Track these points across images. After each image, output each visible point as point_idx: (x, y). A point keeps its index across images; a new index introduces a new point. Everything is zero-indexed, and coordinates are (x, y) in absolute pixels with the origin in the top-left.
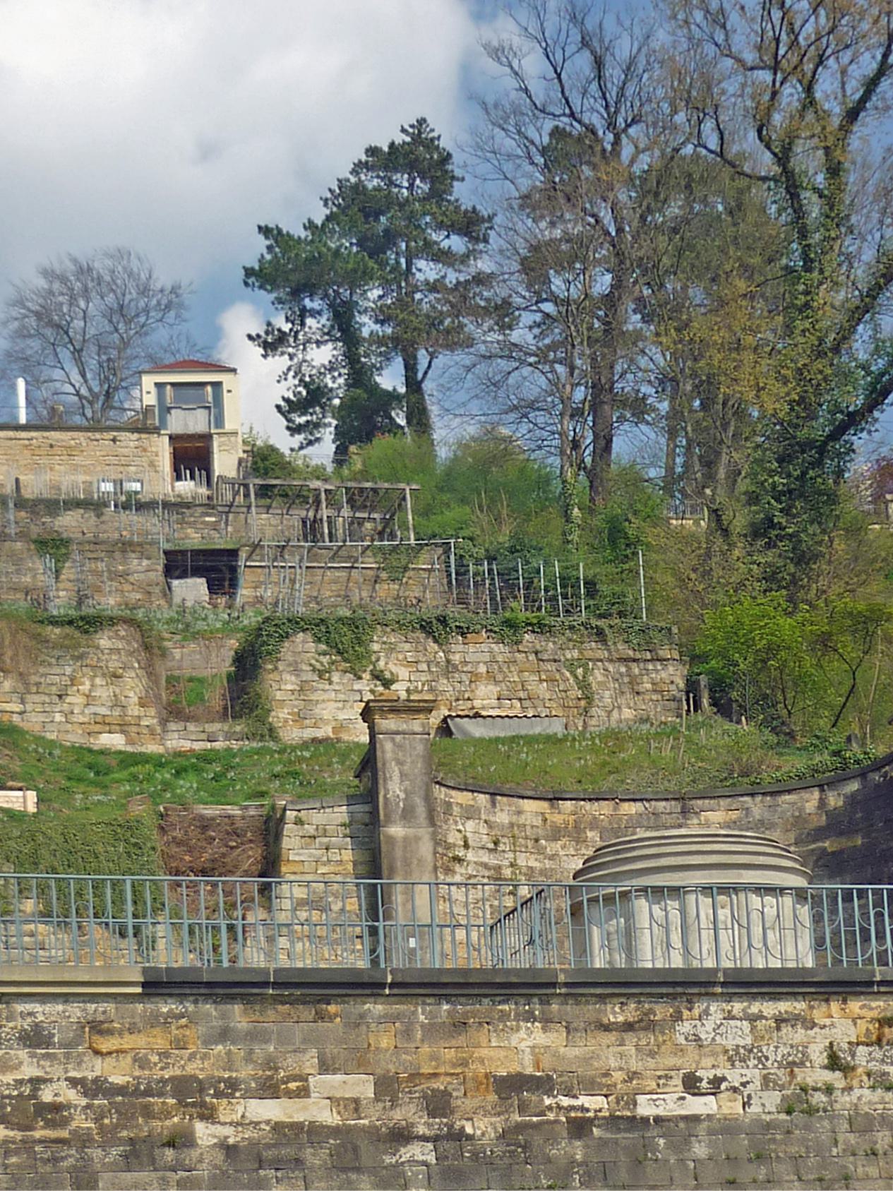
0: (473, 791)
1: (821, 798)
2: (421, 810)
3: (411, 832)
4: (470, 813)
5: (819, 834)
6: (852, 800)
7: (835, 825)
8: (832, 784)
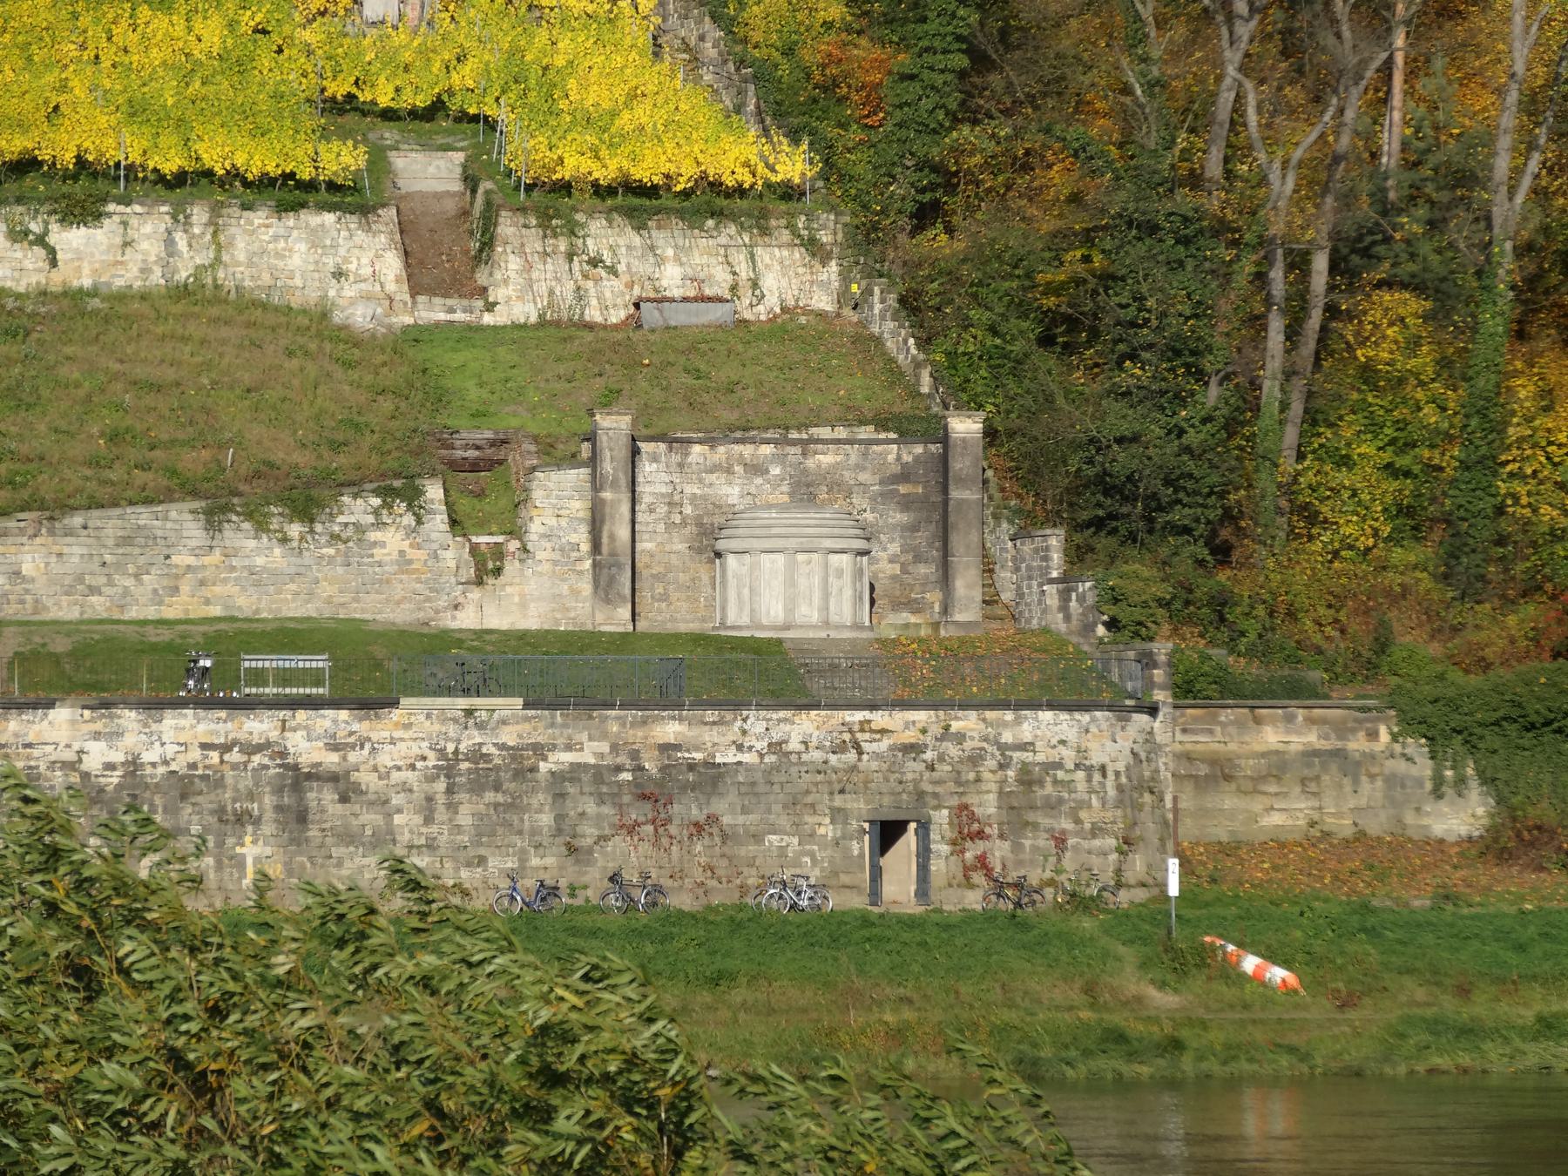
4: (655, 458)
6: (917, 459)
7: (905, 476)
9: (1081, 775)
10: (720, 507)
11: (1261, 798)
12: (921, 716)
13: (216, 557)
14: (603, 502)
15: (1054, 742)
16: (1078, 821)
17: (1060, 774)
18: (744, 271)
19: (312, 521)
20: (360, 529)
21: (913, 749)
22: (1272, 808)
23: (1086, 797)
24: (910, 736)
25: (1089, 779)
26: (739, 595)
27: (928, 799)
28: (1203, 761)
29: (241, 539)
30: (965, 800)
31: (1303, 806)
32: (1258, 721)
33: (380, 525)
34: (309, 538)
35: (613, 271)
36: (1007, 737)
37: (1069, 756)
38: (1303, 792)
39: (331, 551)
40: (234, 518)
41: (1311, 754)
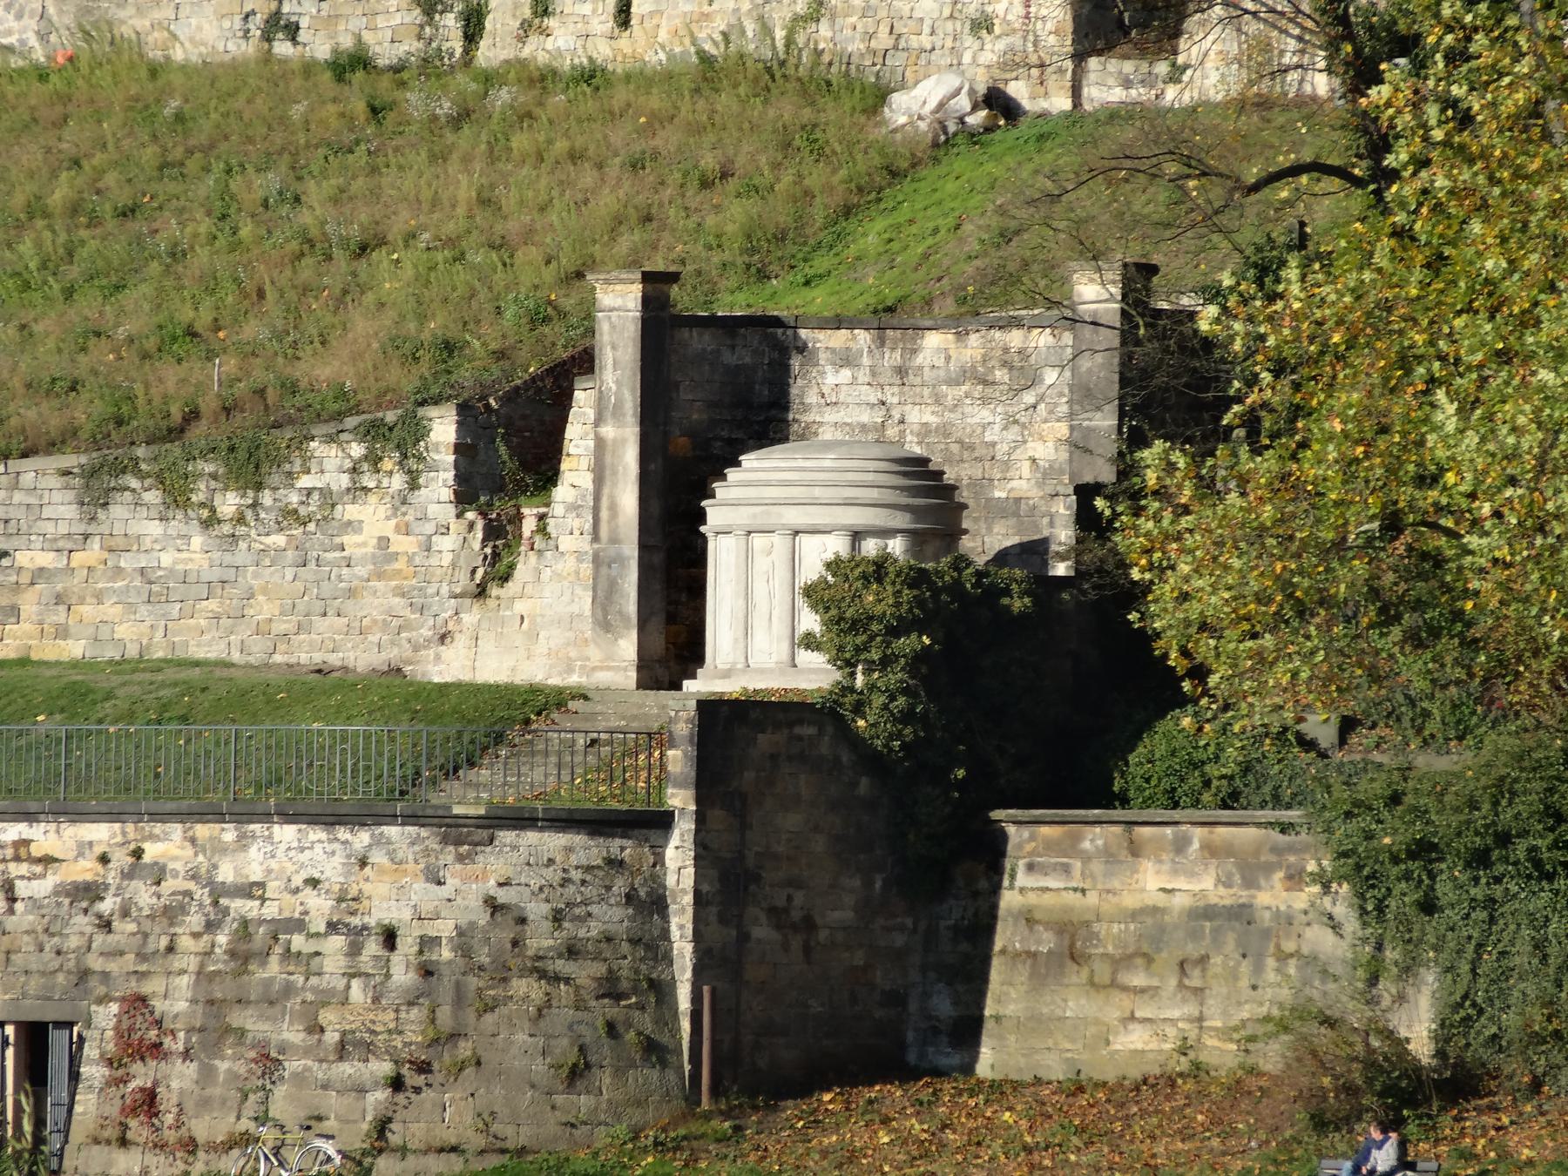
4: (846, 359)
9: (338, 942)
10: (971, 448)
11: (1118, 998)
12: (101, 833)
13: (93, 553)
15: (298, 881)
16: (317, 1029)
17: (298, 942)
19: (259, 487)
20: (329, 499)
21: (88, 892)
22: (1132, 1018)
23: (341, 984)
24: (86, 869)
25: (354, 950)
27: (93, 982)
28: (1048, 925)
29: (138, 518)
30: (147, 988)
31: (1176, 1014)
32: (1135, 850)
33: (358, 491)
34: (249, 514)
36: (226, 873)
37: (319, 907)
38: (1181, 986)
39: (279, 540)
40: (134, 483)
41: (1205, 913)
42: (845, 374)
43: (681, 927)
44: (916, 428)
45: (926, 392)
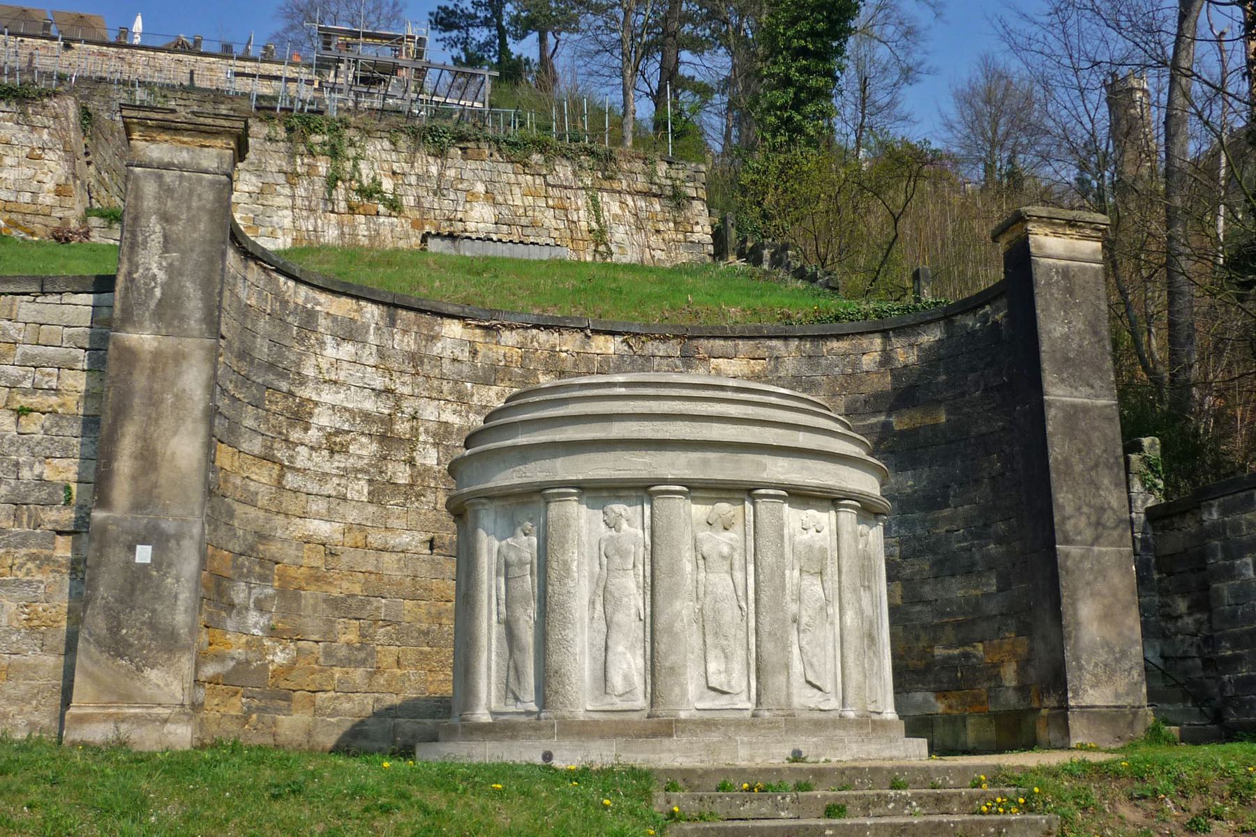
0: (358, 298)
1: (884, 350)
2: (194, 304)
3: (169, 343)
4: (349, 332)
5: (877, 402)
6: (932, 359)
7: (906, 394)
8: (902, 330)
14: (129, 356)
18: (583, 219)
26: (509, 627)
35: (394, 206)
42: (347, 350)
43: (507, 568)
44: (433, 427)
45: (446, 387)
